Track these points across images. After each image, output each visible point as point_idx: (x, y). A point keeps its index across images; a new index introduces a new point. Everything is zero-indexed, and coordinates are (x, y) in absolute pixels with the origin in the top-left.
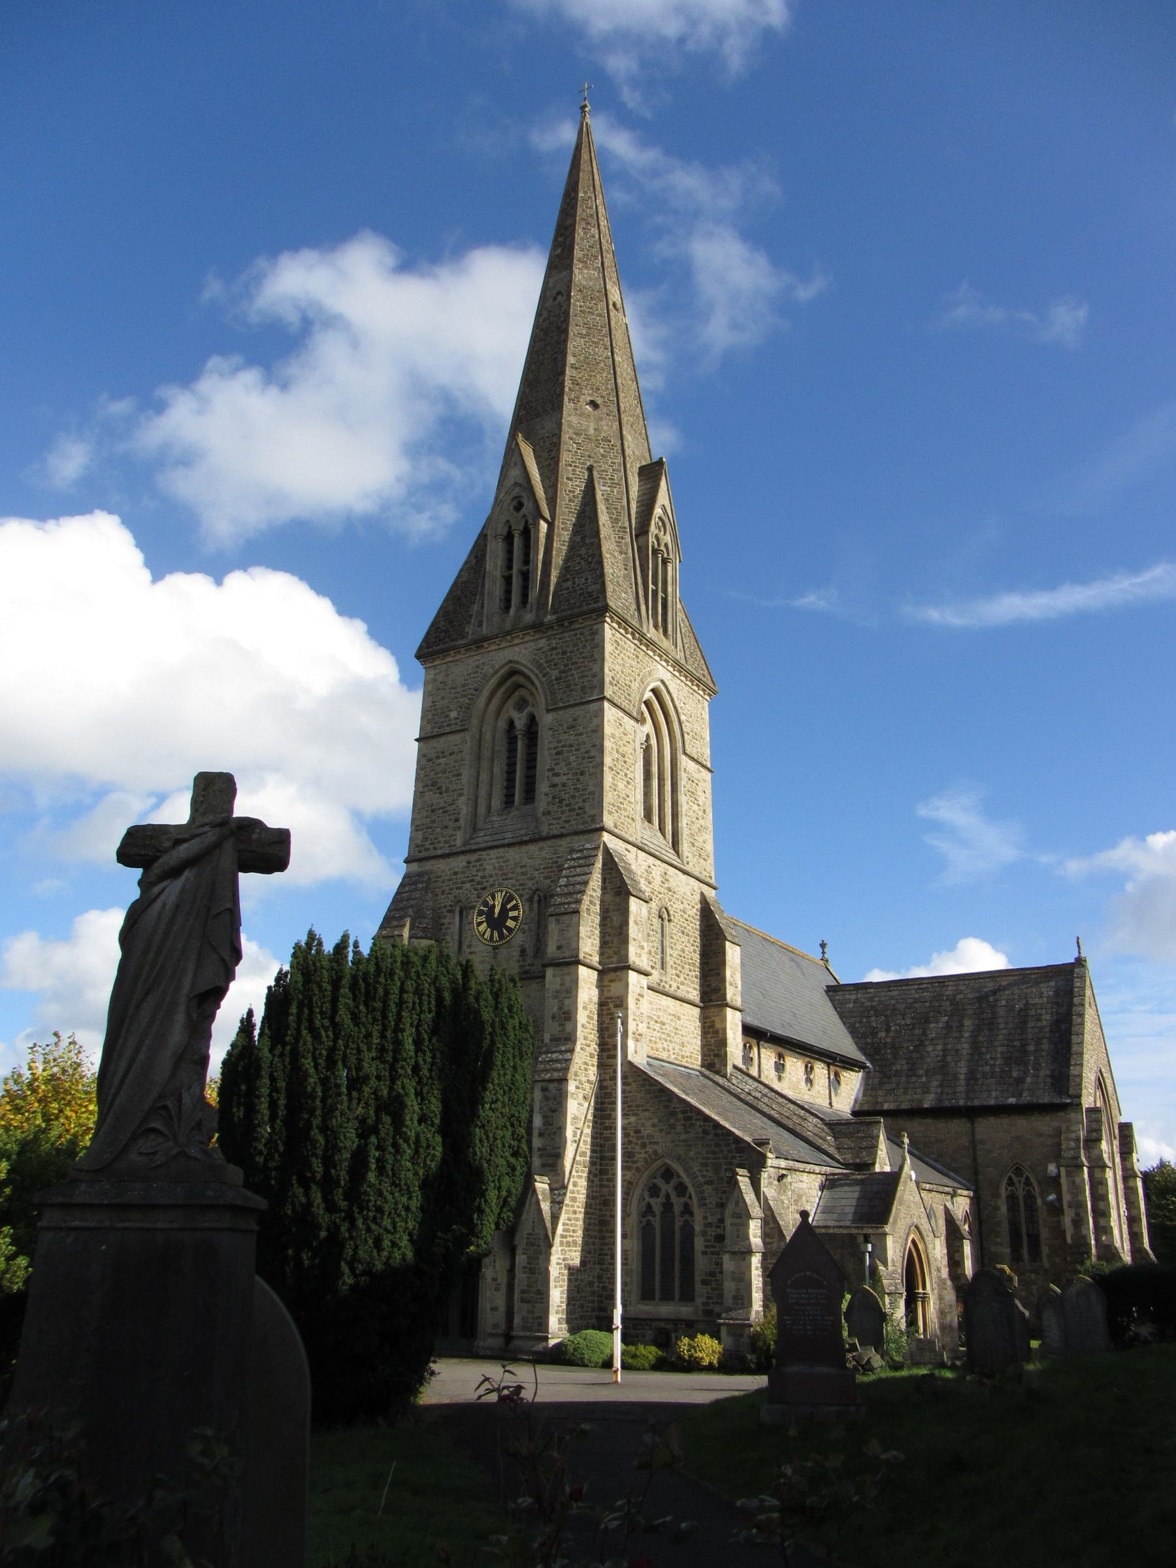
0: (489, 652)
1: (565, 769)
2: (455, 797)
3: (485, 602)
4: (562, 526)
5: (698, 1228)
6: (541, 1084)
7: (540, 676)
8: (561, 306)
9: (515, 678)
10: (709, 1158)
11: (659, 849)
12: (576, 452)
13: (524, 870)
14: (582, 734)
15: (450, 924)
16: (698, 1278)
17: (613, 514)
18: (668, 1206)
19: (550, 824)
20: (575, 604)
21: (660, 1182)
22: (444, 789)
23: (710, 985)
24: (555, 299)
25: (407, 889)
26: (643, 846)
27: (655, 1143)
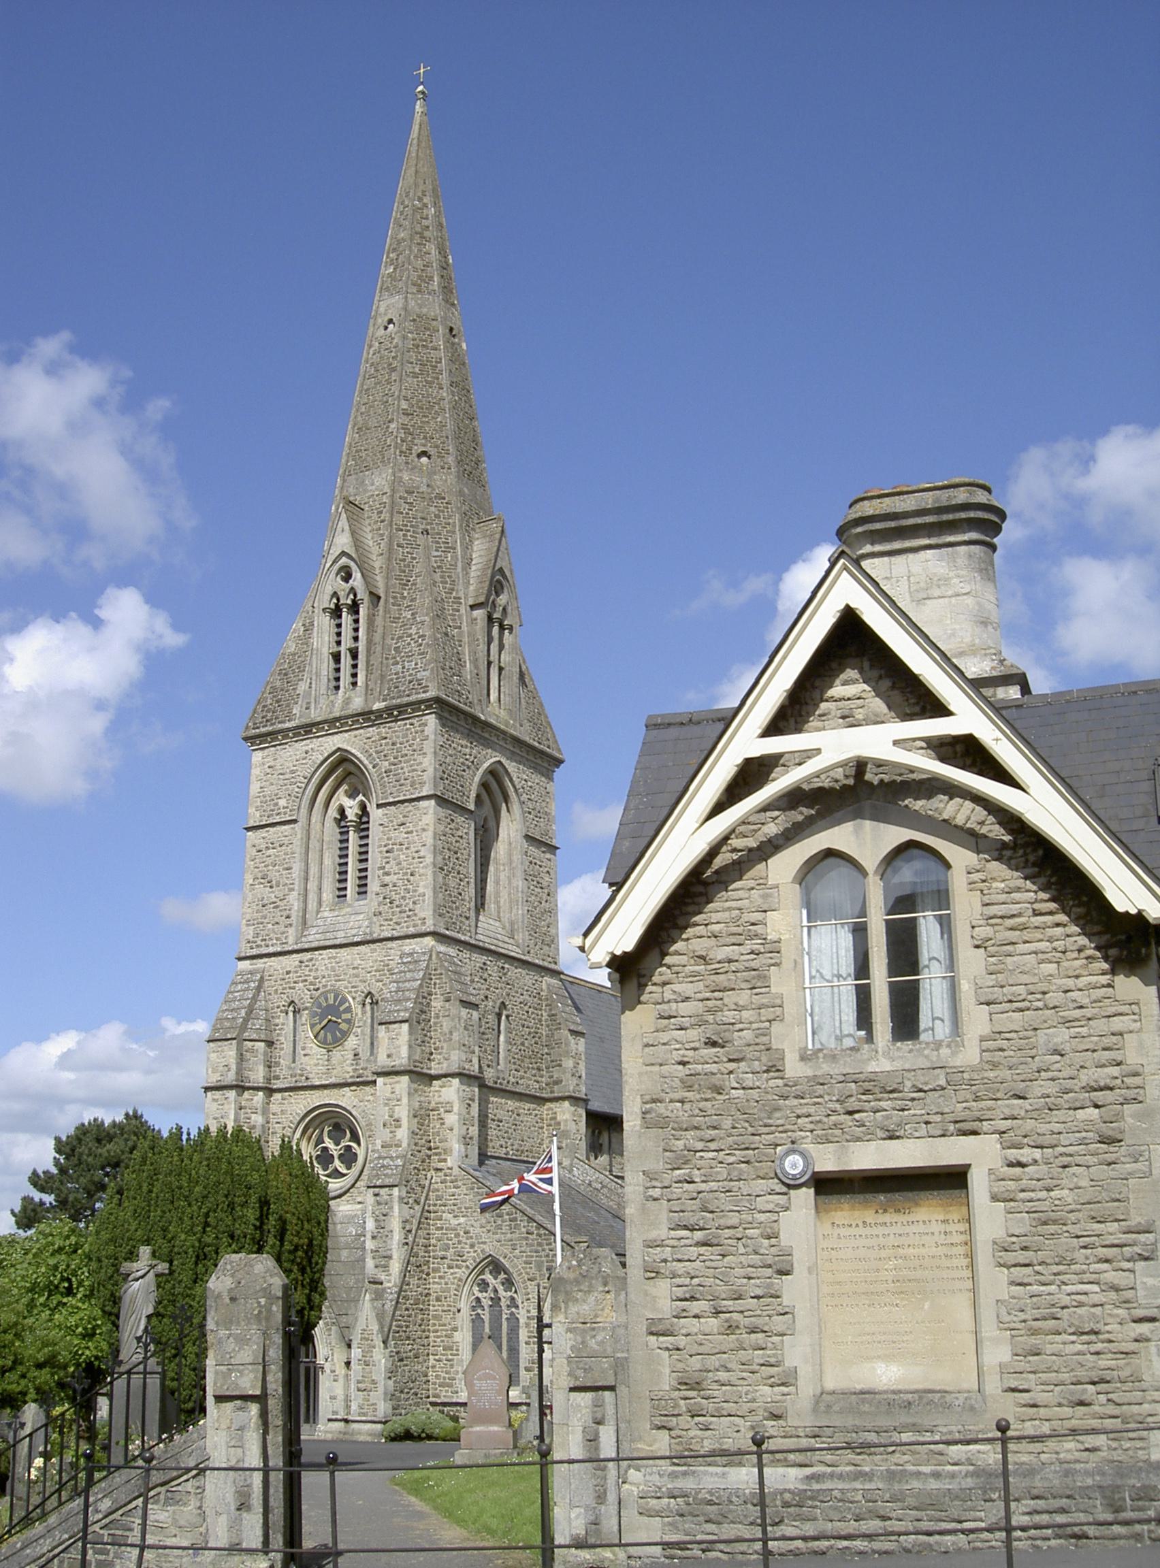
0: (318, 737)
1: (396, 869)
2: (286, 892)
3: (314, 682)
4: (392, 601)
5: (522, 1321)
6: (372, 1190)
7: (370, 767)
8: (393, 339)
9: (346, 765)
10: (532, 1257)
11: (495, 942)
12: (407, 514)
13: (355, 971)
14: (411, 832)
15: (283, 1024)
16: (522, 1365)
17: (446, 583)
18: (496, 1300)
19: (381, 925)
20: (404, 691)
21: (488, 1277)
22: (274, 882)
23: (552, 1077)
24: (386, 328)
25: (239, 987)
26: (477, 943)
27: (484, 1243)
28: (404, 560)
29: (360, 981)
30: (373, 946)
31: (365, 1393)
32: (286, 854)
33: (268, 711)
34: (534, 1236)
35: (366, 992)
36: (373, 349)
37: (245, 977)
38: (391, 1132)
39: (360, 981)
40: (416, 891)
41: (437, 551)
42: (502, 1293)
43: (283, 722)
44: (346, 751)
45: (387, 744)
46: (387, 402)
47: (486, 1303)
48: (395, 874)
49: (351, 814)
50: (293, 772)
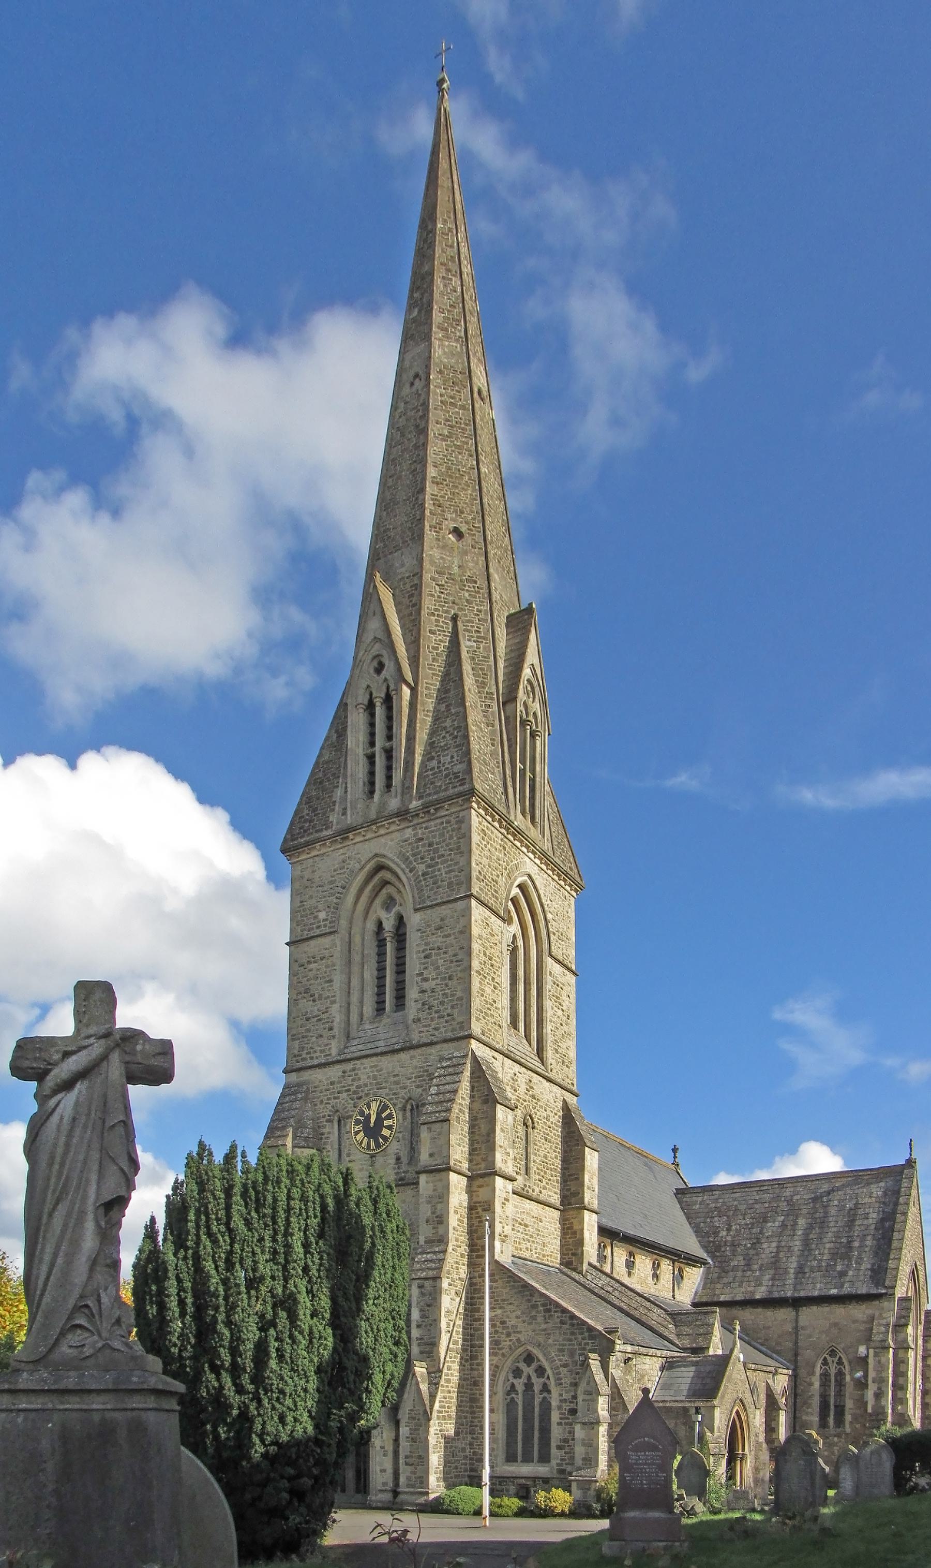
3: (349, 785)
8: (420, 395)
11: (524, 1056)
13: (396, 1079)
15: (329, 1133)
16: (553, 1444)
18: (529, 1386)
19: (420, 1032)
20: (441, 786)
22: (317, 996)
24: (412, 384)
28: (437, 649)
29: (401, 1088)
30: (412, 1052)
31: (413, 1467)
32: (327, 966)
33: (305, 821)
34: (567, 1326)
35: (407, 1098)
36: (399, 411)
37: (293, 1089)
38: (434, 1228)
39: (401, 1088)
40: (453, 995)
41: (469, 640)
42: (534, 1379)
43: (321, 830)
44: (384, 856)
45: (424, 846)
46: (415, 470)
47: (520, 1388)
48: (433, 979)
49: (389, 925)
50: (331, 882)
